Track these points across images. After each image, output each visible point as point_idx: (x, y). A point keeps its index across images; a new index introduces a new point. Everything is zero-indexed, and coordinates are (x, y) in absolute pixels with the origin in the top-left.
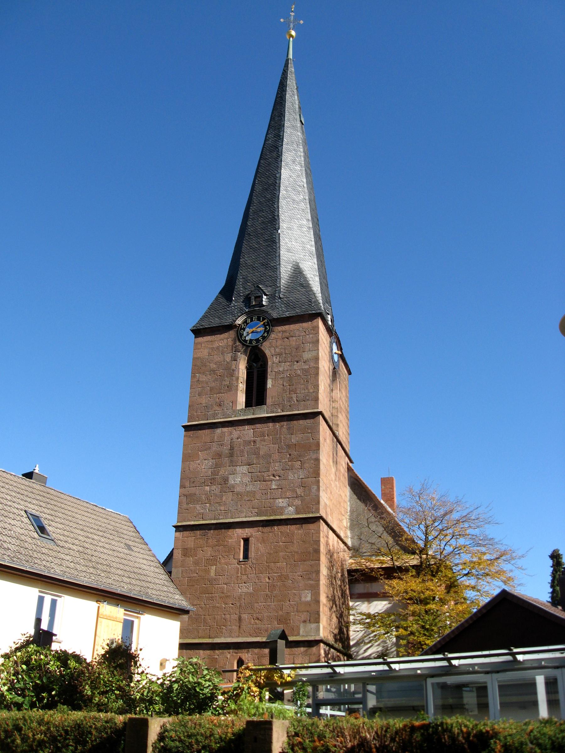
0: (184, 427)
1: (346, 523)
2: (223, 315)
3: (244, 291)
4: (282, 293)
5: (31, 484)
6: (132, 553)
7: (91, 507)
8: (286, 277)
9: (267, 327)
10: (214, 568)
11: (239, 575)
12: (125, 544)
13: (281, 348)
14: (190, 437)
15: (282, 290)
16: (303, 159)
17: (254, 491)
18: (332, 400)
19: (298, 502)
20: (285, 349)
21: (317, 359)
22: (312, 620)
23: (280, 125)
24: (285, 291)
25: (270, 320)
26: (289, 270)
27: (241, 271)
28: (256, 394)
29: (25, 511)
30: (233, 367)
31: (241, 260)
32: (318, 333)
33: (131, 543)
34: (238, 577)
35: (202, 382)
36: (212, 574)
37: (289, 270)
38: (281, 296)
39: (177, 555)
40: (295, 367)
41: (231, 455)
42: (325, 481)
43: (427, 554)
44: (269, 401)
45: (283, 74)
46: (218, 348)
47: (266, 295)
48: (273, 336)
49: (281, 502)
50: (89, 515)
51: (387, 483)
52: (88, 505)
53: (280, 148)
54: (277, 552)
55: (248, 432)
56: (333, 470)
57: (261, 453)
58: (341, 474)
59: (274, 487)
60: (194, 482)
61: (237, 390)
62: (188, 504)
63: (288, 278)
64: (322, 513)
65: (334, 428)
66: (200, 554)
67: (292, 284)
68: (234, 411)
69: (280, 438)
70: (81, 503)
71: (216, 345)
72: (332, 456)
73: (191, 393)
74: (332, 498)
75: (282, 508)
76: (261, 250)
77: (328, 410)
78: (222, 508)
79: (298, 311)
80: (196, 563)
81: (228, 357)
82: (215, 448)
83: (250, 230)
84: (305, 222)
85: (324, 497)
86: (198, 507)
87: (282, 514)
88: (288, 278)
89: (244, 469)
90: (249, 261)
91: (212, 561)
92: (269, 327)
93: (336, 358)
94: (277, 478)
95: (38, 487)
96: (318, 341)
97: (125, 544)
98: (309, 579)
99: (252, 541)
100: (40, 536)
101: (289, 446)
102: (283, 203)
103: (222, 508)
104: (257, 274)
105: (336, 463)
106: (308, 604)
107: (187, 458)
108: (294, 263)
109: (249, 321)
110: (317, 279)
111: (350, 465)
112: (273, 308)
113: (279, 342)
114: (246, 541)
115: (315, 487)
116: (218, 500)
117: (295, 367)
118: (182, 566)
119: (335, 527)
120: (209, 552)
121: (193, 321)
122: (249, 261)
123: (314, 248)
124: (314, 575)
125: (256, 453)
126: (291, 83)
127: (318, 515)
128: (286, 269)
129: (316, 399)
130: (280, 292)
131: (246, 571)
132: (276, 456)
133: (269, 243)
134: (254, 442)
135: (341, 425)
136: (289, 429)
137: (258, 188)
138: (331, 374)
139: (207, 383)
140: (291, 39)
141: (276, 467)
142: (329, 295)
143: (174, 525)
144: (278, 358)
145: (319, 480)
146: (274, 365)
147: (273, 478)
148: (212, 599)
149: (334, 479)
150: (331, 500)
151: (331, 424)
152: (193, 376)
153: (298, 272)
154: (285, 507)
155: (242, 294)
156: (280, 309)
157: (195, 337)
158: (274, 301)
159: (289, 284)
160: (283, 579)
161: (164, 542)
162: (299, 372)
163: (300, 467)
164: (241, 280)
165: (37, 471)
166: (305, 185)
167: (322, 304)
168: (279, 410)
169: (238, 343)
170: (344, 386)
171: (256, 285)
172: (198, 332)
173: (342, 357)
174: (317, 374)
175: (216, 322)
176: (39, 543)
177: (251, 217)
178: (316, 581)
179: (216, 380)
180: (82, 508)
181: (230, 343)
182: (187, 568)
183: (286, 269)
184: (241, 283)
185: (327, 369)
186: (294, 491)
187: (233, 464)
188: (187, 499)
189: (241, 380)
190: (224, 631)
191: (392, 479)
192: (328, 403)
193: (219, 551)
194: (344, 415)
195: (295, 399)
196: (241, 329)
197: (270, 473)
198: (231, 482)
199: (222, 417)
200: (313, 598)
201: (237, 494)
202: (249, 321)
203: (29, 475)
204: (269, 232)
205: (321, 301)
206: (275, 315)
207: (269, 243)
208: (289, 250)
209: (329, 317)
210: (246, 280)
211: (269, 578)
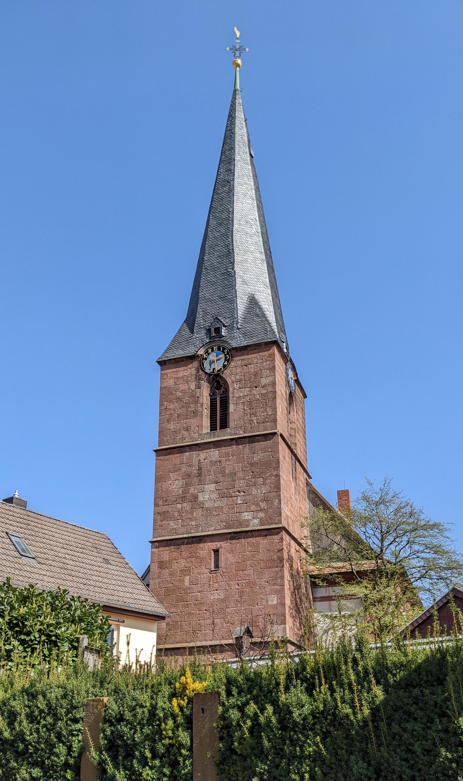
0: (155, 451)
1: (306, 532)
2: (186, 347)
3: (204, 323)
4: (239, 324)
5: (11, 509)
6: (109, 566)
7: (71, 527)
8: (243, 308)
9: (227, 356)
10: (187, 578)
11: (211, 583)
12: (104, 559)
13: (241, 375)
14: (161, 460)
15: (239, 321)
16: (254, 192)
17: (222, 507)
18: (290, 422)
19: (261, 515)
20: (244, 376)
21: (274, 384)
22: (279, 622)
23: (230, 159)
24: (242, 322)
25: (229, 350)
26: (245, 301)
27: (200, 305)
28: (220, 419)
29: (7, 533)
30: (198, 394)
31: (200, 294)
32: (274, 359)
33: (109, 557)
34: (210, 585)
35: (170, 409)
36: (187, 583)
37: (245, 301)
38: (239, 327)
39: (155, 568)
40: (254, 392)
41: (200, 475)
42: (286, 496)
43: (382, 559)
44: (232, 424)
45: (231, 106)
46: (182, 377)
47: (225, 326)
48: (233, 364)
49: (246, 516)
50: (69, 534)
51: (343, 495)
52: (67, 525)
53: (232, 183)
54: (244, 561)
55: (214, 454)
56: (293, 485)
57: (227, 472)
58: (301, 489)
59: (239, 502)
60: (166, 501)
61: (202, 415)
62: (162, 521)
63: (245, 309)
64: (284, 524)
65: (293, 447)
66: (175, 566)
67: (249, 315)
68: (200, 435)
69: (243, 457)
70: (61, 524)
71: (180, 375)
72: (291, 472)
73: (160, 420)
74: (292, 510)
75: (248, 520)
76: (218, 284)
77: (286, 430)
78: (193, 523)
79: (255, 340)
80: (172, 574)
81: (193, 386)
82: (184, 469)
83: (207, 264)
84: (258, 255)
85: (285, 510)
86: (171, 523)
87: (247, 526)
88: (245, 309)
89: (213, 487)
90: (208, 295)
91: (186, 571)
92: (229, 356)
93: (292, 382)
94: (242, 494)
95: (18, 511)
96: (274, 367)
97: (104, 559)
98: (275, 584)
99: (222, 551)
100: (21, 555)
101: (252, 465)
102: (237, 237)
103: (193, 523)
104: (215, 306)
105: (295, 478)
106: (275, 607)
107: (159, 479)
108: (250, 295)
109: (210, 351)
110: (272, 309)
111: (310, 480)
112: (233, 338)
113: (239, 370)
114: (216, 551)
115: (277, 501)
116: (190, 516)
117: (254, 392)
118: (159, 577)
119: (296, 536)
120: (182, 563)
121: (159, 354)
122: (208, 295)
123: (268, 280)
124: (279, 580)
125: (223, 473)
126: (240, 115)
127: (281, 526)
128: (242, 301)
129: (275, 421)
130: (237, 323)
131: (217, 579)
132: (240, 474)
133: (226, 277)
134: (220, 462)
135: (298, 444)
136: (251, 449)
137: (213, 222)
138: (288, 397)
139: (174, 410)
140: (238, 69)
141: (241, 484)
142: (283, 324)
143: (150, 540)
144: (238, 384)
145: (280, 494)
146: (236, 392)
147: (238, 494)
148: (187, 606)
149: (294, 493)
150: (292, 512)
151: (290, 444)
152: (161, 405)
153: (253, 302)
154: (250, 520)
155: (202, 327)
156: (239, 339)
157: (162, 370)
158: (232, 332)
159: (246, 315)
160: (251, 585)
161: (140, 556)
162: (258, 397)
163: (262, 483)
164: (201, 313)
165: (16, 496)
166: (257, 219)
167: (277, 333)
168: (242, 432)
169: (201, 372)
170: (300, 408)
171: (215, 317)
172: (162, 363)
173: (297, 381)
174: (275, 398)
175: (180, 353)
176: (21, 562)
177: (207, 252)
178: (281, 586)
179: (183, 407)
180: (62, 528)
181: (194, 372)
182: (163, 580)
183: (242, 301)
184: (201, 316)
185: (284, 393)
186: (258, 505)
187: (201, 482)
188: (161, 516)
189: (205, 406)
190: (199, 635)
191: (347, 491)
192: (286, 424)
193: (192, 562)
194: (301, 435)
195: (255, 421)
196: (203, 359)
197: (235, 490)
198: (201, 499)
199: (189, 440)
200: (279, 601)
201: (207, 509)
202: (210, 351)
203: (9, 500)
204: (225, 266)
205: (276, 330)
206: (234, 344)
207: (226, 277)
208: (244, 282)
209: (284, 344)
210: (205, 313)
211: (238, 585)
